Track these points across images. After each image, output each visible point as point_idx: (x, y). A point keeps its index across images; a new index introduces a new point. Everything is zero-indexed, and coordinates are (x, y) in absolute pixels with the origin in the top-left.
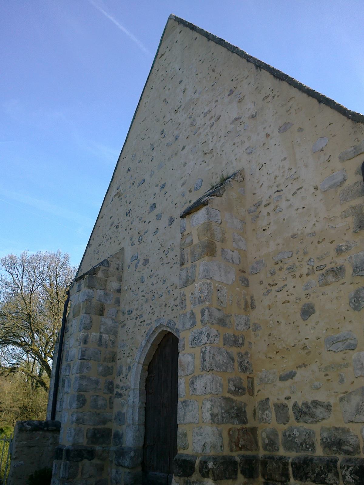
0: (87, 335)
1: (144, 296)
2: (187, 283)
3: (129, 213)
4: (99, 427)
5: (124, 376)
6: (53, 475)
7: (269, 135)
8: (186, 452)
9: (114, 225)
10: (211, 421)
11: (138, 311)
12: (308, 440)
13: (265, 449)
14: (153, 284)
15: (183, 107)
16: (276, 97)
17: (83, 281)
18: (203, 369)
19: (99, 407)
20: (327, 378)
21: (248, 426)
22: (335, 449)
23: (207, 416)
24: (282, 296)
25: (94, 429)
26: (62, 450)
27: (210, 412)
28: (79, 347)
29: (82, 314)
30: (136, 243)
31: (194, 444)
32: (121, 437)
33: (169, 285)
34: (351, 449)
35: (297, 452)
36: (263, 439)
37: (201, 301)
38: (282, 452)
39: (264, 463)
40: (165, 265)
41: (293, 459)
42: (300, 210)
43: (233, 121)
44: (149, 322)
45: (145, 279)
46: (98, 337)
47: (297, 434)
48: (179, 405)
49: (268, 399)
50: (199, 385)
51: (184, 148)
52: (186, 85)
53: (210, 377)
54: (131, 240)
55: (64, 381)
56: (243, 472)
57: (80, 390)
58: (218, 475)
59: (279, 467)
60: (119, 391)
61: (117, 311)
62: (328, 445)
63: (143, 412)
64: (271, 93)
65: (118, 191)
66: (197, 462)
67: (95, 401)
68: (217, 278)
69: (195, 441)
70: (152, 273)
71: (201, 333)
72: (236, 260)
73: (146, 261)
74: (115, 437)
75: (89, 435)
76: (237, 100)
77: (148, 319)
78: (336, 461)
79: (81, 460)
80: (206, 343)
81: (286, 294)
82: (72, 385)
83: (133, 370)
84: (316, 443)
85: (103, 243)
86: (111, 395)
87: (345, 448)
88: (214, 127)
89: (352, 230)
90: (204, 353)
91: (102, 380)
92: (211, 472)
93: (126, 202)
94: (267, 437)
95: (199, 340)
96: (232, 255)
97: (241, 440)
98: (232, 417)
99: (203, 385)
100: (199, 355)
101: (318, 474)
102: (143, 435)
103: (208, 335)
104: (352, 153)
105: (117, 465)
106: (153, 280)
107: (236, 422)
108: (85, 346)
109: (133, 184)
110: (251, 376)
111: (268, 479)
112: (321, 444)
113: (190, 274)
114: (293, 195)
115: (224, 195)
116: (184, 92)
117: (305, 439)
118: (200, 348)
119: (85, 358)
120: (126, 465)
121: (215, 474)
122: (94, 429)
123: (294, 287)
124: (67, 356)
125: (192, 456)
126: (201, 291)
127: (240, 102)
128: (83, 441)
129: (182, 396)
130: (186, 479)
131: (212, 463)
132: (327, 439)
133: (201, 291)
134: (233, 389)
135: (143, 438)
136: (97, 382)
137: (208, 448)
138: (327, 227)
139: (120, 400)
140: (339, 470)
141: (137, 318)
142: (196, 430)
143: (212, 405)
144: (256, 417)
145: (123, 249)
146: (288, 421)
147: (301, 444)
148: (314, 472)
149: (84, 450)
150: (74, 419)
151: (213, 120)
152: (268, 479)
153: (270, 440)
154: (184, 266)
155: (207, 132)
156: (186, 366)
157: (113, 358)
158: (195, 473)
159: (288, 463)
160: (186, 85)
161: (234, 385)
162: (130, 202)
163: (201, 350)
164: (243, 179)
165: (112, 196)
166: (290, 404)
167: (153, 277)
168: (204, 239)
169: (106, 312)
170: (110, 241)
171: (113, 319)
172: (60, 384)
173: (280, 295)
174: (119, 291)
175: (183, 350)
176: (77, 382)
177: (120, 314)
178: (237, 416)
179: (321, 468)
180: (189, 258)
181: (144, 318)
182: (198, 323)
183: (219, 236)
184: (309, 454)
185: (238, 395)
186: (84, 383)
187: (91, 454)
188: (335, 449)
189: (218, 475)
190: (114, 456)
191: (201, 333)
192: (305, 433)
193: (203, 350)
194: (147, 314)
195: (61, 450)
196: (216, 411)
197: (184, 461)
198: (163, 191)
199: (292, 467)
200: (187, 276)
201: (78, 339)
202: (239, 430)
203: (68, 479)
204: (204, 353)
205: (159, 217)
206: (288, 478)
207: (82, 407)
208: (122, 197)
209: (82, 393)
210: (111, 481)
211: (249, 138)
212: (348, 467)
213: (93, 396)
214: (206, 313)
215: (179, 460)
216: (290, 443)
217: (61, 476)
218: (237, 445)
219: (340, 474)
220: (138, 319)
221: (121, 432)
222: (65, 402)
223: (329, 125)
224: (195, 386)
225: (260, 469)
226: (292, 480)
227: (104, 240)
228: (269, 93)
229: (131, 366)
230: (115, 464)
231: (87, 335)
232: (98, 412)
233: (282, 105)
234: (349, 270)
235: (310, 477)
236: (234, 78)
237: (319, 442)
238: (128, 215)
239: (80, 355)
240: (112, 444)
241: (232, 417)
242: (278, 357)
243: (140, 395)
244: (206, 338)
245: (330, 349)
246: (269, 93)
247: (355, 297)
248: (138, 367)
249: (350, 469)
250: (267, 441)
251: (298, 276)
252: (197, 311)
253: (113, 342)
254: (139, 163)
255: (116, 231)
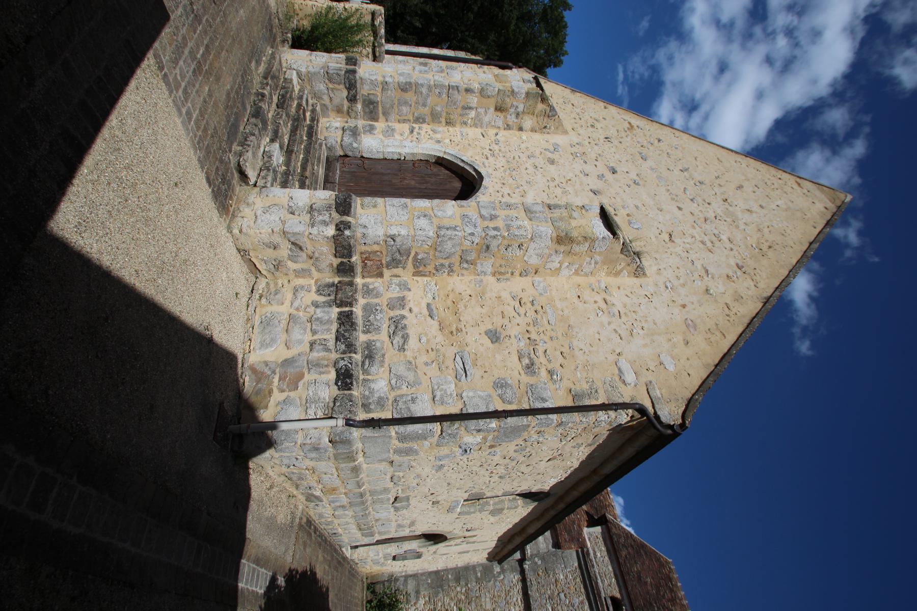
0: (474, 93)
1: (514, 158)
2: (528, 211)
3: (609, 141)
4: (380, 108)
5: (431, 135)
6: (330, 54)
7: (684, 308)
8: (359, 206)
9: (595, 122)
10: (388, 234)
11: (498, 152)
12: (373, 328)
13: (364, 285)
14: (526, 169)
15: (730, 209)
16: (728, 318)
17: (534, 85)
18: (440, 228)
19: (400, 108)
20: (430, 350)
21: (385, 270)
22: (366, 352)
23: (393, 231)
24: (509, 311)
25: (377, 103)
26: (355, 64)
27: (397, 234)
28: (462, 83)
29: (498, 86)
30: (574, 150)
31: (366, 215)
32: (371, 133)
33: (525, 188)
34: (366, 367)
35: (362, 316)
36: (373, 283)
37: (508, 228)
38: (362, 301)
39: (351, 284)
40: (547, 184)
41: (355, 312)
42: (597, 336)
43: (705, 268)
44: (487, 165)
45: (532, 160)
46: (471, 105)
47: (378, 318)
48: (403, 200)
49: (410, 290)
50: (423, 222)
51: (680, 209)
52: (756, 213)
53: (431, 234)
54: (577, 144)
55: (425, 65)
56: (342, 263)
57: (417, 84)
58: (338, 240)
59: (348, 298)
60: (416, 130)
61: (499, 128)
62: (369, 346)
63: (396, 157)
64: (733, 313)
65: (635, 127)
66: (349, 219)
67: (406, 103)
68: (533, 245)
69: (369, 217)
70: (538, 168)
71: (475, 226)
72: (549, 265)
73: (552, 162)
74: (371, 126)
75: (372, 97)
76: (731, 274)
77: (489, 163)
78: (355, 353)
79: (346, 87)
80: (465, 232)
81: (511, 316)
82: (422, 75)
83: (437, 147)
84: (371, 335)
85: (575, 109)
86: (412, 121)
87: (367, 362)
88: (701, 246)
89: (573, 387)
90: (455, 229)
91: (426, 110)
92: (340, 233)
93: (622, 138)
94: (375, 287)
95: (468, 224)
96: (555, 262)
97: (372, 262)
98: (393, 255)
99: (424, 227)
100: (453, 223)
101: (344, 336)
102: (373, 157)
103: (472, 234)
104: (655, 394)
105: (343, 128)
106: (531, 170)
107: (389, 259)
108: (463, 91)
109: (642, 146)
110: (432, 274)
111: (337, 287)
112: (369, 340)
113: (537, 215)
114: (615, 330)
115: (623, 256)
116: (749, 210)
117: (374, 325)
118: (460, 225)
119: (451, 90)
120: (344, 138)
121: (338, 237)
122: (377, 103)
123: (518, 325)
124: (452, 68)
125: (355, 214)
126: (518, 228)
127: (728, 276)
128: (364, 90)
129: (412, 204)
130: (334, 207)
131: (349, 234)
132: (374, 345)
133: (519, 227)
134: (419, 257)
135: (371, 157)
136: (424, 105)
137: (364, 230)
138: (578, 362)
139: (407, 132)
140: (349, 355)
141: (490, 150)
142: (379, 218)
143: (404, 236)
144: (393, 278)
145: (565, 132)
146: (390, 308)
147: (369, 321)
148: (345, 331)
149: (356, 91)
150: (387, 79)
151: (709, 244)
152: (337, 287)
153: (373, 290)
154: (547, 209)
155: (695, 237)
156: (442, 208)
157: (450, 123)
158: (340, 216)
159: (352, 307)
160: (756, 213)
161: (423, 259)
162: (621, 142)
163: (458, 226)
164: (637, 277)
165: (630, 120)
166: (405, 312)
167: (534, 170)
168: (575, 234)
169: (499, 114)
170: (577, 117)
171: (490, 123)
172: (422, 60)
173: (511, 309)
174: (521, 129)
175: (458, 206)
176: (426, 82)
177: (495, 131)
178: (393, 260)
179: (349, 338)
180: (555, 215)
181: (491, 159)
182: (486, 223)
183: (576, 248)
184: (360, 327)
185: (413, 261)
186: (424, 90)
187: (352, 99)
188: (366, 352)
189: (338, 240)
190: (352, 125)
191: (475, 226)
192: (379, 324)
193: (458, 228)
194: (494, 163)
195: (355, 64)
196: (398, 239)
197: (350, 205)
198: (631, 183)
199: (348, 311)
200: (536, 212)
201: (471, 82)
202: (381, 261)
203: (327, 73)
204: (455, 229)
205: (601, 177)
206: (339, 306)
207: (400, 88)
208: (628, 132)
209: (414, 88)
210: (329, 121)
211: (683, 285)
212: (351, 364)
213: (411, 100)
214: (496, 233)
215: (351, 199)
216: (369, 310)
217: (330, 64)
218: (366, 259)
219: (344, 356)
220: (490, 152)
221: (376, 132)
222: (404, 67)
223: (689, 374)
224: (422, 218)
225: (346, 279)
226: (338, 310)
227: (578, 110)
228: (734, 310)
229: (442, 144)
230: (344, 126)
231: (474, 93)
232: (395, 106)
233: (717, 325)
234: (532, 380)
235: (340, 328)
236: (758, 271)
237: (372, 338)
238: (606, 140)
239: (454, 84)
240: (364, 122)
241: (393, 255)
242: (449, 303)
243: (413, 154)
244: (470, 232)
245: (457, 355)
246: (734, 310)
247: (506, 383)
248: (440, 151)
249: (350, 366)
250: (371, 287)
251: (528, 329)
252: (500, 223)
253: (465, 123)
254: (668, 153)
255: (589, 125)
